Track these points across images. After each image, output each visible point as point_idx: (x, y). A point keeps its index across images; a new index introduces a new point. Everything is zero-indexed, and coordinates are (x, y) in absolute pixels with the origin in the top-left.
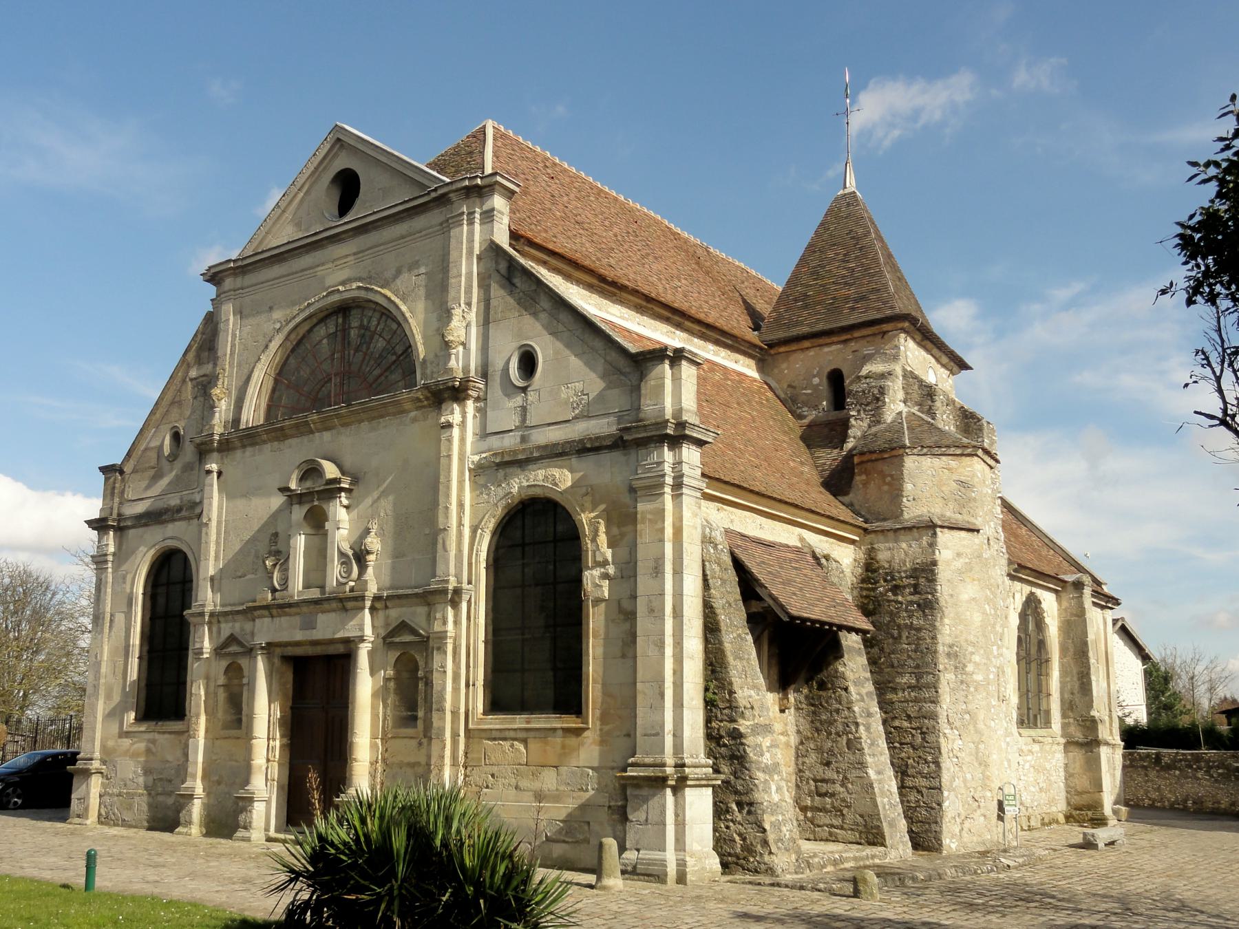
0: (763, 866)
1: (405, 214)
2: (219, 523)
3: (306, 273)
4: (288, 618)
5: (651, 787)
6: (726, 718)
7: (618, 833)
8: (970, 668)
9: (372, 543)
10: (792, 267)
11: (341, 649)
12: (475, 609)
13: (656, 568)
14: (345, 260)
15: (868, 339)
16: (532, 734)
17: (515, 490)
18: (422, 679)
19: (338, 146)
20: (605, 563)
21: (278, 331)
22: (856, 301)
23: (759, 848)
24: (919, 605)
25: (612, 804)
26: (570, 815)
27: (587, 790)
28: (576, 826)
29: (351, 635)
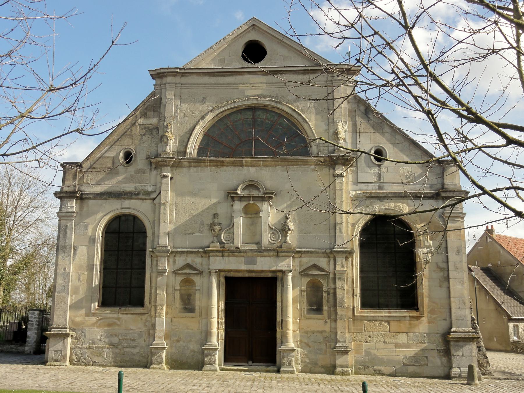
0: (487, 372)
2: (172, 204)
3: (230, 85)
4: (235, 258)
5: (465, 341)
7: (443, 361)
12: (355, 261)
13: (458, 251)
14: (260, 85)
16: (392, 319)
17: (377, 210)
18: (325, 292)
19: (252, 27)
23: (485, 365)
25: (439, 348)
26: (416, 354)
27: (425, 343)
28: (420, 358)
29: (283, 269)
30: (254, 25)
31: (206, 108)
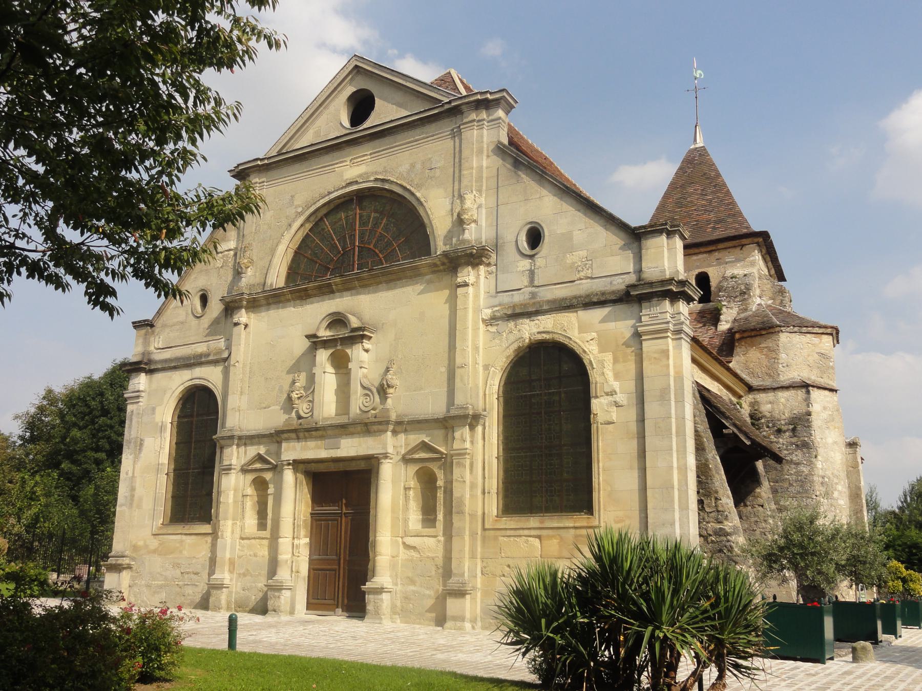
1: (419, 122)
6: (712, 520)
8: (836, 494)
9: (392, 379)
10: (660, 199)
11: (362, 465)
15: (729, 250)
19: (355, 71)
20: (612, 393)
21: (301, 214)
22: (715, 222)
24: (797, 445)
30: (356, 66)
31: (294, 211)
